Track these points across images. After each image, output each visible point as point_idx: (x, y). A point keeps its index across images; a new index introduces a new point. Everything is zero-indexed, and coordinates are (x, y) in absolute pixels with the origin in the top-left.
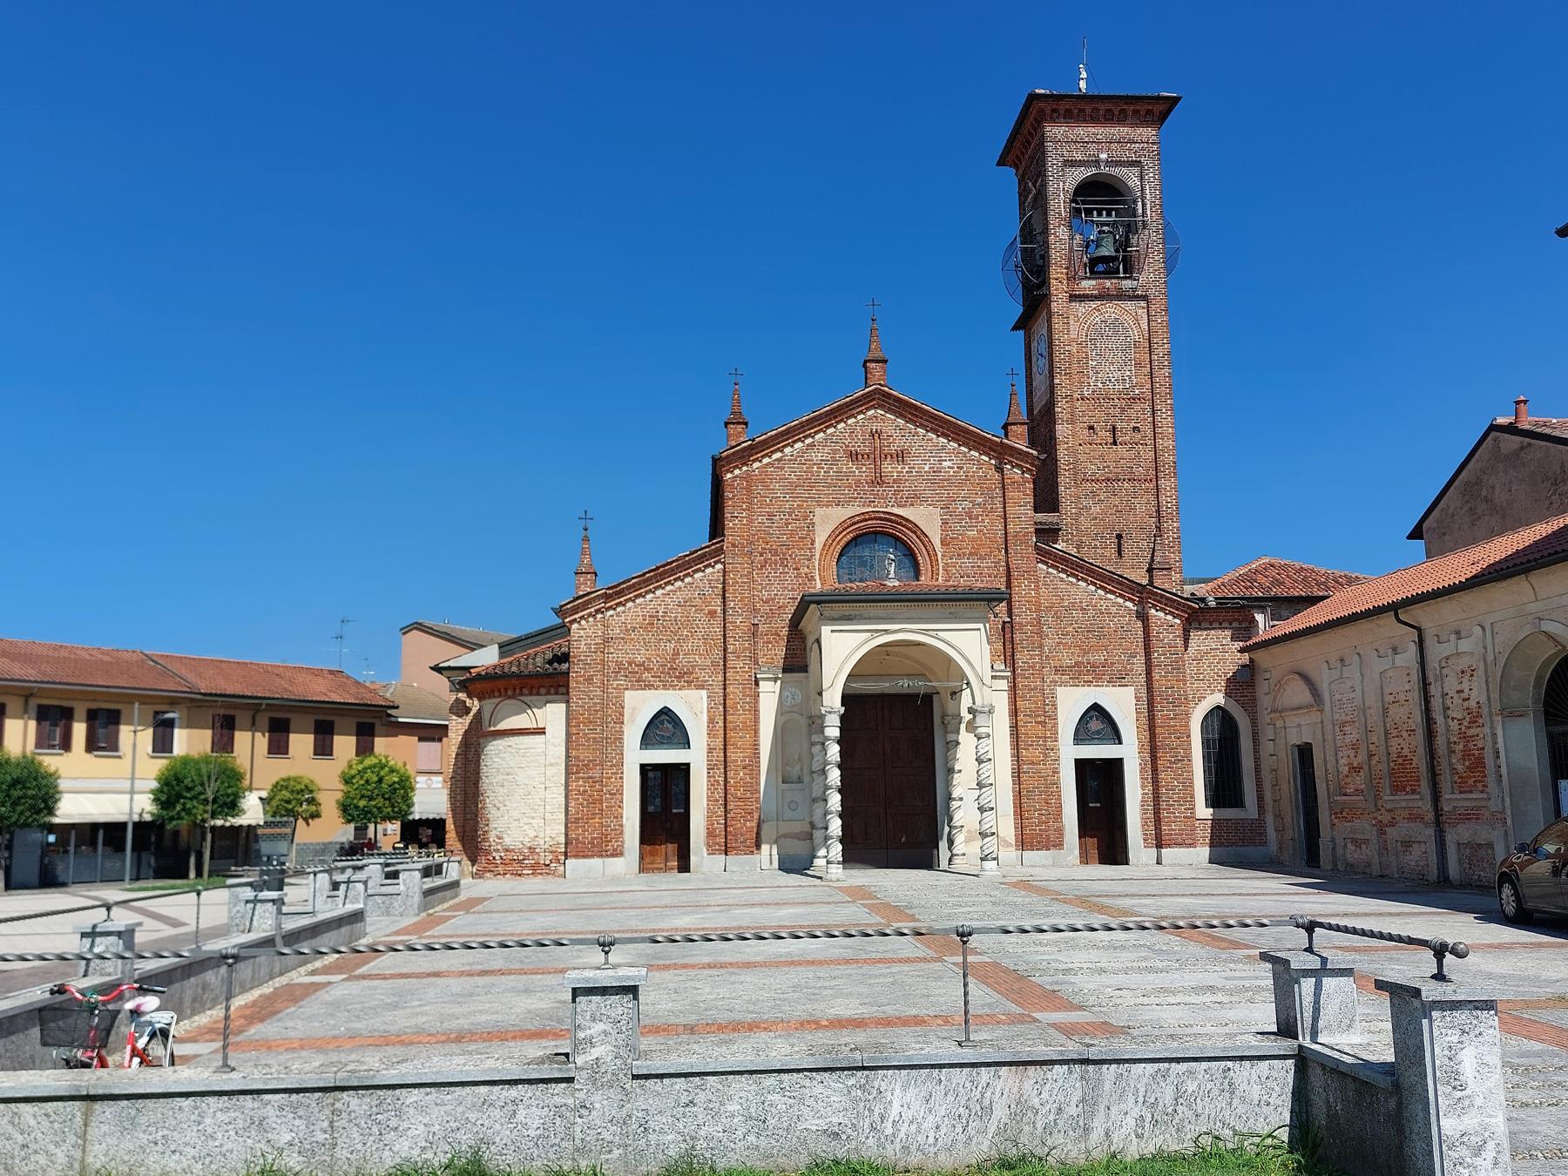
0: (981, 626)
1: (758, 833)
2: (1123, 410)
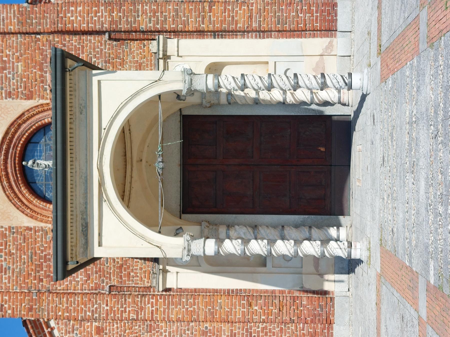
0: (95, 80)
1: (314, 292)
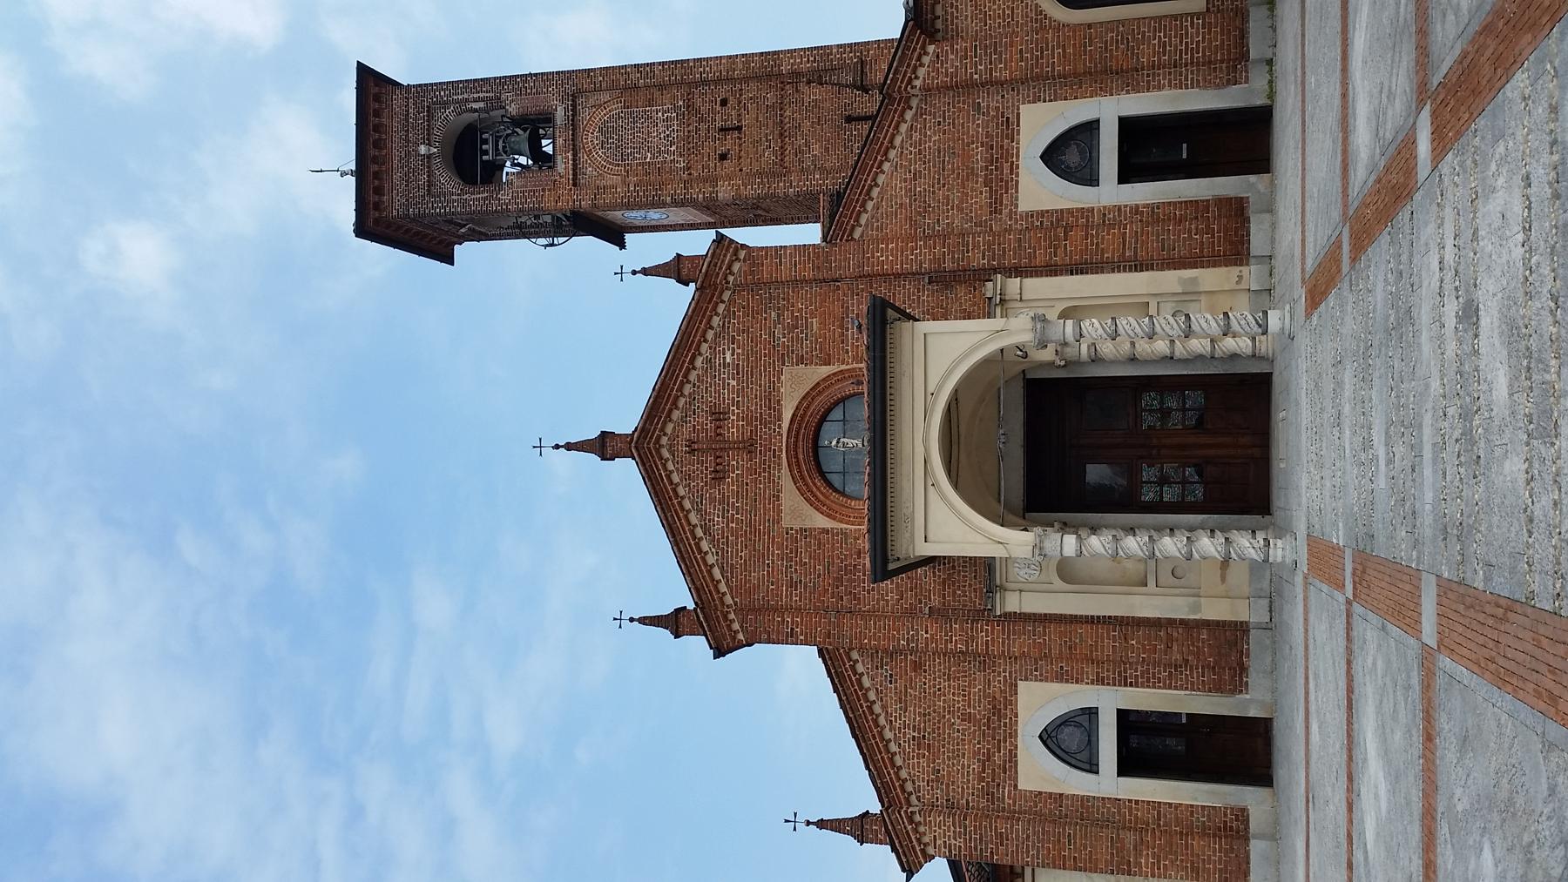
2: (701, 120)
